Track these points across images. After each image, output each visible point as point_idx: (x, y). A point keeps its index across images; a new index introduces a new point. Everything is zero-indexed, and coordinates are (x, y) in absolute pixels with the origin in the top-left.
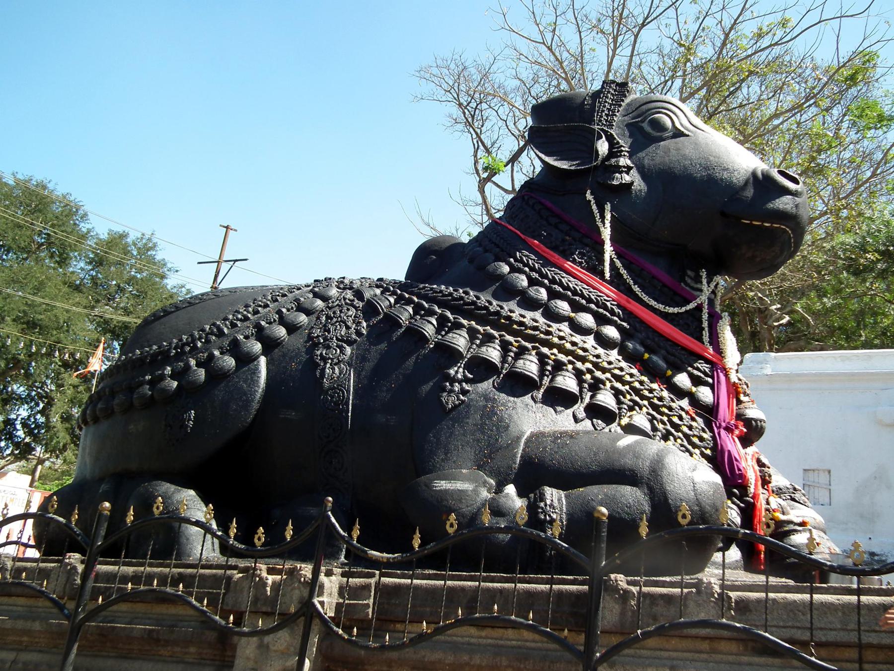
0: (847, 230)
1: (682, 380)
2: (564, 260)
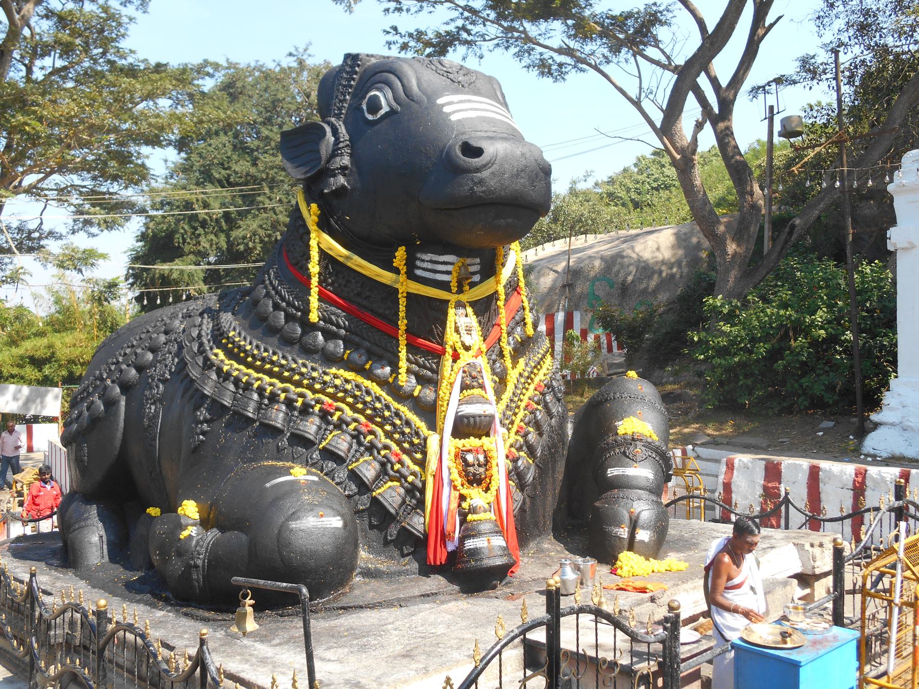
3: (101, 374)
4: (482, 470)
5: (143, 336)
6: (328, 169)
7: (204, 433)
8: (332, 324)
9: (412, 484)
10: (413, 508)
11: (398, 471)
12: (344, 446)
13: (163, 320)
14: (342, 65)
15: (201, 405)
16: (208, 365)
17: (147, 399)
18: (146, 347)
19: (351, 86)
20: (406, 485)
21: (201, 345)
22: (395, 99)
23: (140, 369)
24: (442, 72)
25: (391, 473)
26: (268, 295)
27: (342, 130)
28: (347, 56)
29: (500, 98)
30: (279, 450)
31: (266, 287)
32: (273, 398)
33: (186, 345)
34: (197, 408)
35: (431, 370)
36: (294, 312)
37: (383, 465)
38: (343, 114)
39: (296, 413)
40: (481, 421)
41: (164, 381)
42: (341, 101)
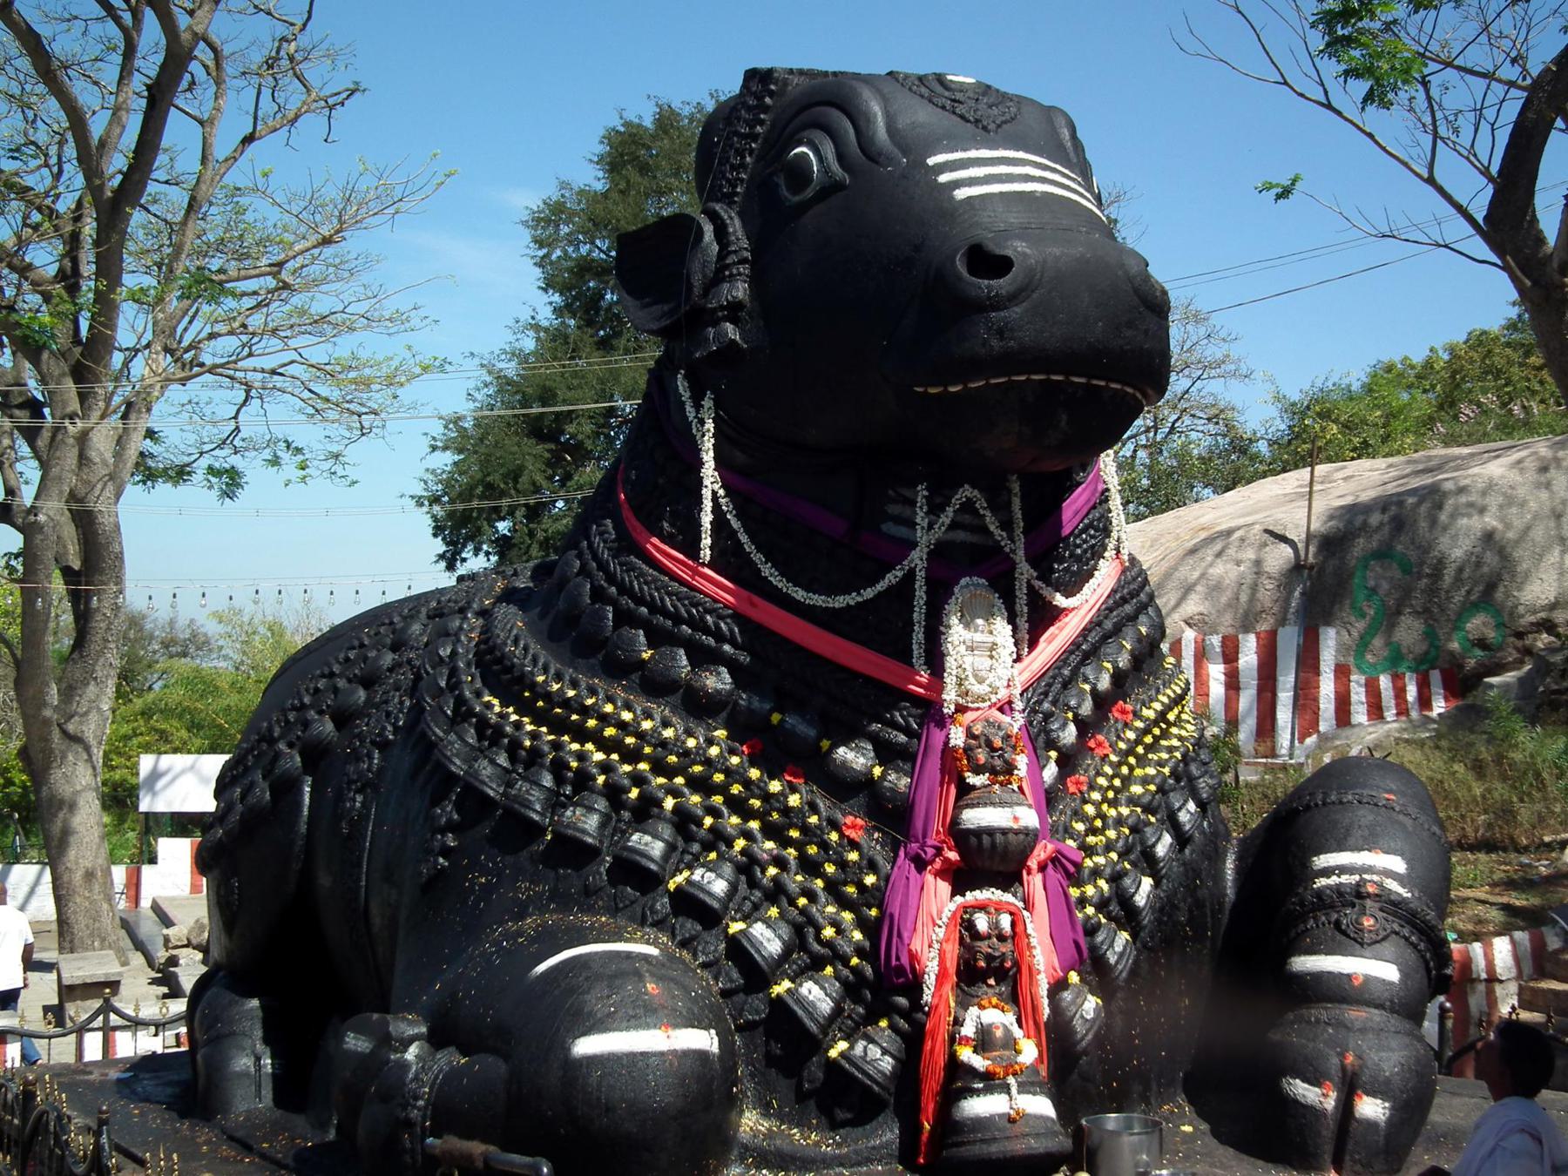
0: (1497, 378)
1: (854, 757)
2: (645, 533)
3: (270, 729)
4: (1006, 948)
5: (352, 655)
6: (703, 310)
7: (446, 852)
8: (707, 631)
9: (855, 970)
10: (857, 1025)
11: (828, 944)
12: (719, 887)
13: (392, 623)
14: (741, 94)
15: (444, 797)
16: (463, 713)
17: (350, 782)
18: (355, 675)
19: (754, 137)
20: (846, 972)
21: (454, 672)
22: (841, 157)
23: (343, 719)
24: (941, 101)
25: (816, 947)
26: (584, 571)
27: (736, 227)
28: (752, 75)
29: (1072, 155)
30: (588, 892)
31: (580, 556)
32: (583, 781)
33: (428, 673)
34: (437, 800)
35: (907, 730)
36: (632, 605)
37: (798, 930)
38: (737, 194)
39: (626, 815)
40: (1006, 846)
41: (384, 746)
42: (733, 168)
